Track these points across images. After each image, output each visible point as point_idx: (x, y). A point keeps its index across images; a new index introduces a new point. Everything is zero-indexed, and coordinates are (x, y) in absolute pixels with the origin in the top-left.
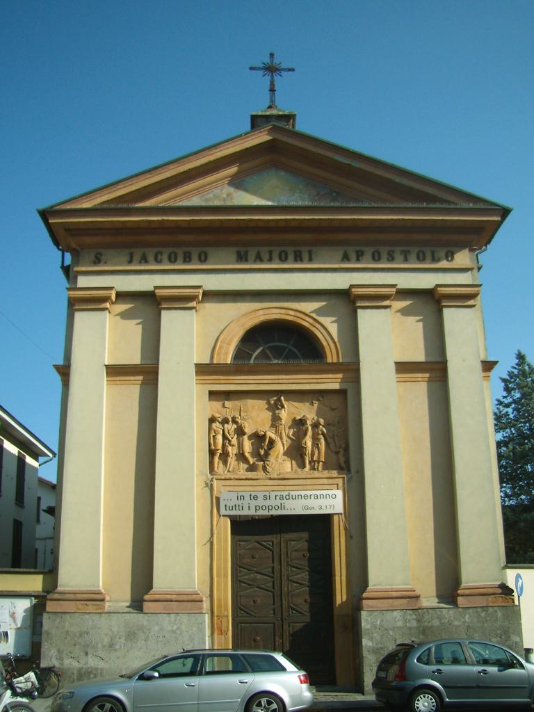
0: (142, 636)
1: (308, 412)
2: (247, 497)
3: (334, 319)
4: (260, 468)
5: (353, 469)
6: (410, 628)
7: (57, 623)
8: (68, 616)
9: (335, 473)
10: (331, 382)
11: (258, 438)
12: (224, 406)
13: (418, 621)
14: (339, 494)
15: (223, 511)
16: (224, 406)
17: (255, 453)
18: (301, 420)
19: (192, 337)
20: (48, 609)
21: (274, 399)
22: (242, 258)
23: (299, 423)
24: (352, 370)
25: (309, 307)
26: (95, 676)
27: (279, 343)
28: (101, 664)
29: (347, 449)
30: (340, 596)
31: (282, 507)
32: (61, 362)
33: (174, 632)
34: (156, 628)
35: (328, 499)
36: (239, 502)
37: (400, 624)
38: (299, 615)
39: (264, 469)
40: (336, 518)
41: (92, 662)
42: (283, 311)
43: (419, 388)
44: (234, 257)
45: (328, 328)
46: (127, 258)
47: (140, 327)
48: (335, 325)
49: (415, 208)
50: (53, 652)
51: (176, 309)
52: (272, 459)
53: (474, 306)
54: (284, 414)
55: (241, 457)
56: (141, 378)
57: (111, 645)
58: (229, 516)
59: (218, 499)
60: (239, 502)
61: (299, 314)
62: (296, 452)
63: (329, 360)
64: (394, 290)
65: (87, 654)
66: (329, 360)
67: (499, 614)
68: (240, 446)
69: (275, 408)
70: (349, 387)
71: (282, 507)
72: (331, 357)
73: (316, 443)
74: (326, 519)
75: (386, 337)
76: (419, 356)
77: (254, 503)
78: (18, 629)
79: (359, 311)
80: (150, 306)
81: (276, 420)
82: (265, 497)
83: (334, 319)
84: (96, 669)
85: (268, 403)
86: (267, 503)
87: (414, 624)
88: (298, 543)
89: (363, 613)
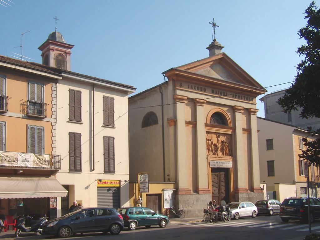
0: (199, 201)
1: (222, 138)
2: (216, 163)
3: (190, 107)
4: (216, 154)
5: (234, 156)
6: (247, 198)
7: (182, 198)
8: (184, 196)
9: (229, 157)
10: (229, 132)
11: (215, 145)
12: (208, 136)
13: (248, 196)
14: (232, 162)
15: (210, 166)
16: (208, 136)
17: (215, 150)
18: (223, 141)
19: (204, 113)
20: (179, 194)
21: (218, 135)
22: (213, 92)
23: (223, 142)
24: (234, 129)
25: (225, 109)
26: (191, 212)
27: (219, 119)
28: (192, 209)
29: (232, 150)
30: (232, 190)
31: (224, 164)
32: (189, 119)
33: (205, 199)
34: (202, 198)
35: (229, 164)
36: (214, 164)
37: (245, 197)
38: (18, 182)
39: (217, 155)
40: (231, 169)
41: (190, 208)
42: (220, 110)
43: (190, 129)
44: (211, 92)
45: (229, 116)
46: (188, 87)
47: (190, 109)
48: (230, 115)
49: (234, 83)
50: (181, 206)
51: (200, 105)
52: (218, 152)
53: (203, 106)
54: (220, 139)
55: (212, 151)
56: (192, 125)
57: (193, 203)
58: (211, 167)
59: (209, 163)
60: (214, 164)
61: (223, 111)
62: (222, 150)
63: (229, 126)
64: (187, 98)
65: (188, 206)
66: (229, 126)
67: (261, 195)
68: (212, 148)
69: (218, 137)
70: (233, 134)
71: (222, 166)
72: (229, 125)
73: (226, 149)
74: (229, 168)
75: (240, 120)
76: (245, 127)
77: (217, 164)
78: (170, 200)
79: (197, 106)
80: (194, 103)
81: (218, 140)
82: (218, 163)
83: (190, 107)
84: (191, 210)
85: (217, 136)
86: (220, 164)
87: (247, 197)
88: (222, 174)
89: (239, 194)
